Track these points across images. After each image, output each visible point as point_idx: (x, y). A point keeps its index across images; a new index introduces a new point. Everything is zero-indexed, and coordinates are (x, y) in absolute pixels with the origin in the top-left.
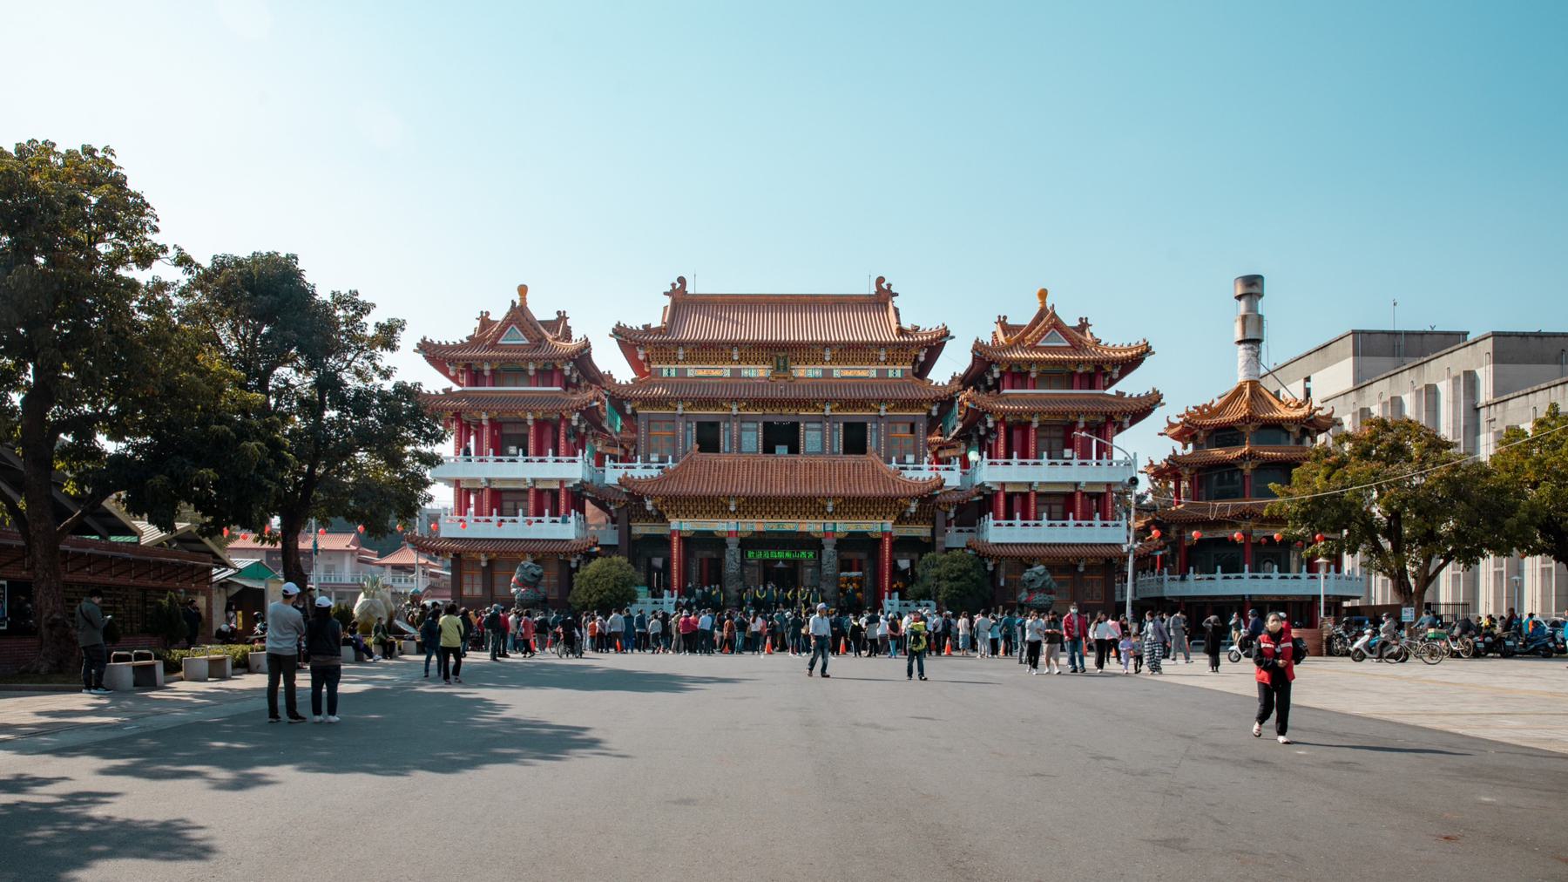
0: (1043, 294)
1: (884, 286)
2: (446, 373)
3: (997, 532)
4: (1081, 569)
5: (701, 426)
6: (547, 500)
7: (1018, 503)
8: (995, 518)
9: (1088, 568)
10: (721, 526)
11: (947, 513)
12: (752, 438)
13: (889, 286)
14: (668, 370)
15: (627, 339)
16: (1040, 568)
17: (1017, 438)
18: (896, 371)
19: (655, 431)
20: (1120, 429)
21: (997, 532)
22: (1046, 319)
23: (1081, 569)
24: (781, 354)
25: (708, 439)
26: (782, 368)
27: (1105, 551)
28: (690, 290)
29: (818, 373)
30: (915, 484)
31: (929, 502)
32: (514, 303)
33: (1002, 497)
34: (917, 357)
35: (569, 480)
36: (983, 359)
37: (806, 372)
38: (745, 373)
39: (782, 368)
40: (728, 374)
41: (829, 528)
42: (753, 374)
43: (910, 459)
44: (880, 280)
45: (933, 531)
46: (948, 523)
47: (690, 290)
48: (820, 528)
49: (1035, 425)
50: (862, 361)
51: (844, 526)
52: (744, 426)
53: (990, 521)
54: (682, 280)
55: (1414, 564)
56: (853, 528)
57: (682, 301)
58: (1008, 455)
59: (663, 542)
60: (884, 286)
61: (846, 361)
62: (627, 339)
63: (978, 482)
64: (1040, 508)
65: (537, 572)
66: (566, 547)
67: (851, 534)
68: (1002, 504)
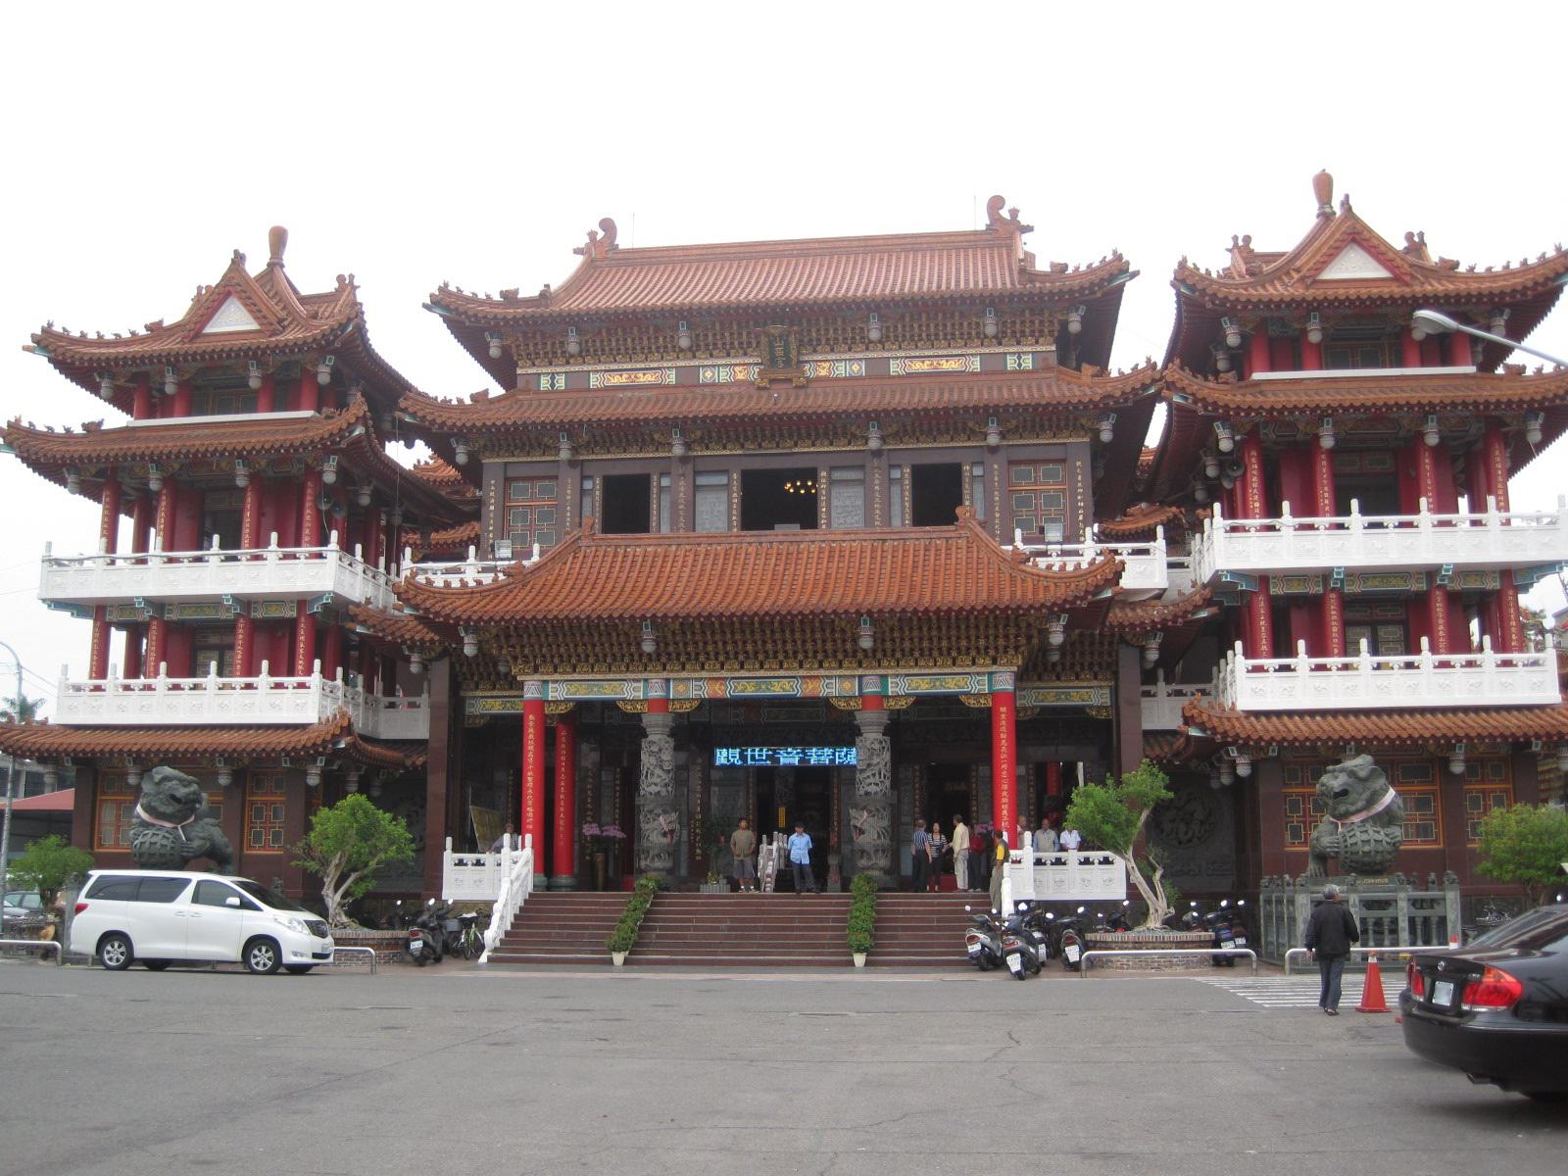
0: (1323, 185)
1: (1005, 213)
2: (94, 389)
3: (1257, 687)
4: (1458, 768)
5: (611, 485)
6: (271, 636)
7: (1297, 615)
8: (1249, 653)
9: (1474, 764)
10: (630, 689)
11: (1143, 650)
12: (718, 510)
13: (1014, 212)
14: (552, 379)
15: (471, 322)
16: (1362, 763)
17: (1290, 466)
18: (1021, 358)
19: (519, 501)
20: (1522, 455)
21: (1257, 687)
22: (1343, 230)
23: (1458, 768)
24: (775, 330)
25: (626, 507)
26: (781, 364)
27: (1512, 723)
28: (624, 241)
29: (857, 368)
30: (1063, 577)
31: (1096, 624)
32: (238, 259)
33: (1261, 606)
34: (1064, 324)
35: (319, 595)
36: (1202, 310)
37: (837, 369)
38: (707, 376)
39: (781, 364)
40: (671, 378)
41: (871, 688)
42: (724, 376)
43: (1054, 533)
44: (996, 203)
45: (1115, 693)
46: (1149, 677)
47: (624, 241)
48: (850, 688)
49: (1327, 442)
50: (950, 340)
51: (905, 684)
52: (701, 480)
53: (1237, 661)
54: (608, 225)
55: (350, 837)
56: (924, 686)
57: (603, 255)
58: (1273, 511)
59: (512, 726)
60: (1005, 213)
61: (915, 341)
62: (471, 322)
63: (1206, 576)
64: (1351, 632)
65: (182, 792)
66: (303, 738)
67: (921, 701)
68: (1263, 624)
